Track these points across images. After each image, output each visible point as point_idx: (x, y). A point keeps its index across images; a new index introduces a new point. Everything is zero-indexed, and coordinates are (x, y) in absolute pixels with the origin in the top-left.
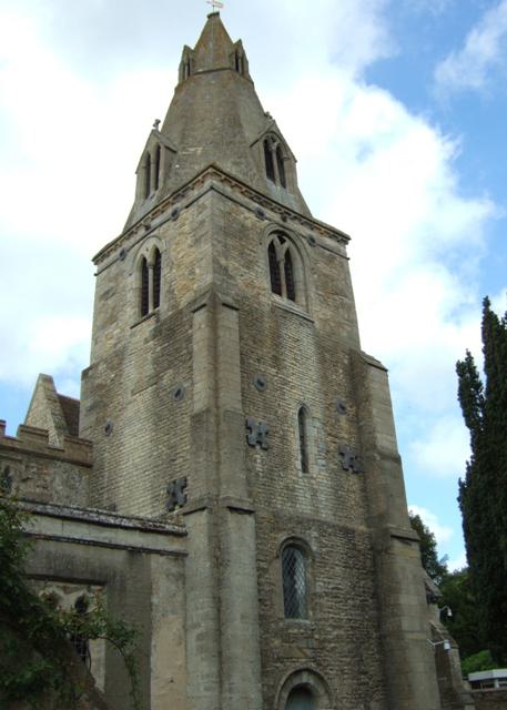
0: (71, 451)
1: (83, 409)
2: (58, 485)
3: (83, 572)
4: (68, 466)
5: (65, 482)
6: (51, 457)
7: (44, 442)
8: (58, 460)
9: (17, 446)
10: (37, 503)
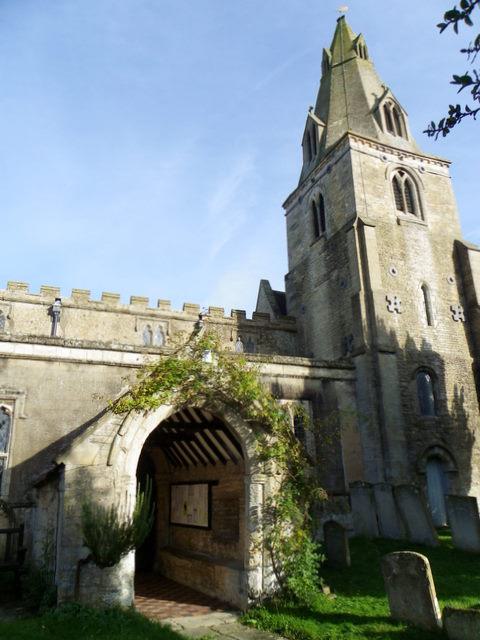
1: (288, 300)
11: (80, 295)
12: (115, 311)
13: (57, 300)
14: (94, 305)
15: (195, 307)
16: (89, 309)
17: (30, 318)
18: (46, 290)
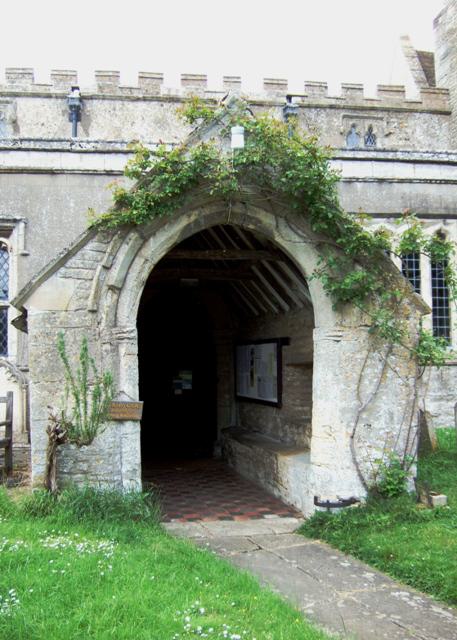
0: (429, 101)
1: (437, 59)
2: (419, 135)
3: (437, 208)
4: (427, 116)
5: (426, 132)
6: (410, 110)
7: (401, 97)
8: (416, 111)
9: (376, 105)
10: (388, 151)
11: (107, 77)
12: (158, 99)
13: (73, 89)
14: (127, 93)
15: (282, 84)
16: (121, 98)
17: (43, 119)
18: (61, 76)
